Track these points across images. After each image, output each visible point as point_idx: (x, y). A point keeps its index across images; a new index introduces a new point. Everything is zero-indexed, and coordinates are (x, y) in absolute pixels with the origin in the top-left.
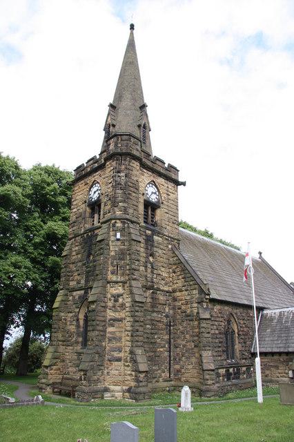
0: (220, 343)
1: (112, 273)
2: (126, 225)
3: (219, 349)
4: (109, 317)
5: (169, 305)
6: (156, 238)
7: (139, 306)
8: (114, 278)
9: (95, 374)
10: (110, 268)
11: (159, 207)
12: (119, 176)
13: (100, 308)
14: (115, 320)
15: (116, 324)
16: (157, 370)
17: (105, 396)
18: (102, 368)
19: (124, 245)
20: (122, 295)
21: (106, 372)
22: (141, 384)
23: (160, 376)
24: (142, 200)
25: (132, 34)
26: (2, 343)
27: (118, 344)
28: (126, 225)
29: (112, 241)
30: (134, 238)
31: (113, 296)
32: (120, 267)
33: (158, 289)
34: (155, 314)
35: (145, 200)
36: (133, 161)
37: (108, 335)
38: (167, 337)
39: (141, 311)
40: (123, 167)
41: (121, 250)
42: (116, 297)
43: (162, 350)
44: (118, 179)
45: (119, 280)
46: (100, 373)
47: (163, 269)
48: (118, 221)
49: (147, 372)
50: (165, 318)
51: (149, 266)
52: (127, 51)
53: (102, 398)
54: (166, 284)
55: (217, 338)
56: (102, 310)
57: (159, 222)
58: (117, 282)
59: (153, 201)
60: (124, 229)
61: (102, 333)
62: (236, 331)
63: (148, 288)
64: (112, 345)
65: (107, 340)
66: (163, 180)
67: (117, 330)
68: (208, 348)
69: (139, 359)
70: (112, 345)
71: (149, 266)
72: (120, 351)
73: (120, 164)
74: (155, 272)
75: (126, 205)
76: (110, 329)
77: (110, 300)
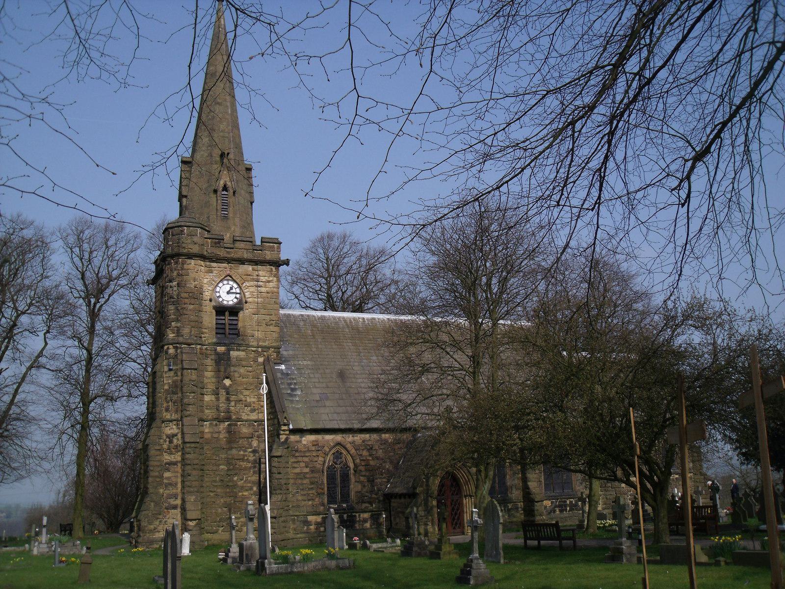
1: (167, 410)
6: (233, 354)
8: (168, 416)
9: (150, 524)
11: (242, 309)
12: (171, 287)
20: (176, 435)
27: (174, 491)
28: (179, 351)
31: (168, 436)
33: (239, 420)
34: (234, 452)
35: (215, 308)
36: (189, 261)
37: (165, 481)
39: (194, 453)
42: (171, 437)
43: (246, 493)
46: (157, 523)
47: (246, 393)
48: (171, 347)
50: (252, 455)
51: (223, 392)
54: (253, 411)
58: (171, 421)
59: (231, 303)
60: (176, 356)
62: (352, 465)
63: (220, 421)
66: (250, 268)
67: (173, 474)
70: (168, 492)
71: (223, 392)
74: (233, 398)
75: (179, 325)
76: (167, 474)
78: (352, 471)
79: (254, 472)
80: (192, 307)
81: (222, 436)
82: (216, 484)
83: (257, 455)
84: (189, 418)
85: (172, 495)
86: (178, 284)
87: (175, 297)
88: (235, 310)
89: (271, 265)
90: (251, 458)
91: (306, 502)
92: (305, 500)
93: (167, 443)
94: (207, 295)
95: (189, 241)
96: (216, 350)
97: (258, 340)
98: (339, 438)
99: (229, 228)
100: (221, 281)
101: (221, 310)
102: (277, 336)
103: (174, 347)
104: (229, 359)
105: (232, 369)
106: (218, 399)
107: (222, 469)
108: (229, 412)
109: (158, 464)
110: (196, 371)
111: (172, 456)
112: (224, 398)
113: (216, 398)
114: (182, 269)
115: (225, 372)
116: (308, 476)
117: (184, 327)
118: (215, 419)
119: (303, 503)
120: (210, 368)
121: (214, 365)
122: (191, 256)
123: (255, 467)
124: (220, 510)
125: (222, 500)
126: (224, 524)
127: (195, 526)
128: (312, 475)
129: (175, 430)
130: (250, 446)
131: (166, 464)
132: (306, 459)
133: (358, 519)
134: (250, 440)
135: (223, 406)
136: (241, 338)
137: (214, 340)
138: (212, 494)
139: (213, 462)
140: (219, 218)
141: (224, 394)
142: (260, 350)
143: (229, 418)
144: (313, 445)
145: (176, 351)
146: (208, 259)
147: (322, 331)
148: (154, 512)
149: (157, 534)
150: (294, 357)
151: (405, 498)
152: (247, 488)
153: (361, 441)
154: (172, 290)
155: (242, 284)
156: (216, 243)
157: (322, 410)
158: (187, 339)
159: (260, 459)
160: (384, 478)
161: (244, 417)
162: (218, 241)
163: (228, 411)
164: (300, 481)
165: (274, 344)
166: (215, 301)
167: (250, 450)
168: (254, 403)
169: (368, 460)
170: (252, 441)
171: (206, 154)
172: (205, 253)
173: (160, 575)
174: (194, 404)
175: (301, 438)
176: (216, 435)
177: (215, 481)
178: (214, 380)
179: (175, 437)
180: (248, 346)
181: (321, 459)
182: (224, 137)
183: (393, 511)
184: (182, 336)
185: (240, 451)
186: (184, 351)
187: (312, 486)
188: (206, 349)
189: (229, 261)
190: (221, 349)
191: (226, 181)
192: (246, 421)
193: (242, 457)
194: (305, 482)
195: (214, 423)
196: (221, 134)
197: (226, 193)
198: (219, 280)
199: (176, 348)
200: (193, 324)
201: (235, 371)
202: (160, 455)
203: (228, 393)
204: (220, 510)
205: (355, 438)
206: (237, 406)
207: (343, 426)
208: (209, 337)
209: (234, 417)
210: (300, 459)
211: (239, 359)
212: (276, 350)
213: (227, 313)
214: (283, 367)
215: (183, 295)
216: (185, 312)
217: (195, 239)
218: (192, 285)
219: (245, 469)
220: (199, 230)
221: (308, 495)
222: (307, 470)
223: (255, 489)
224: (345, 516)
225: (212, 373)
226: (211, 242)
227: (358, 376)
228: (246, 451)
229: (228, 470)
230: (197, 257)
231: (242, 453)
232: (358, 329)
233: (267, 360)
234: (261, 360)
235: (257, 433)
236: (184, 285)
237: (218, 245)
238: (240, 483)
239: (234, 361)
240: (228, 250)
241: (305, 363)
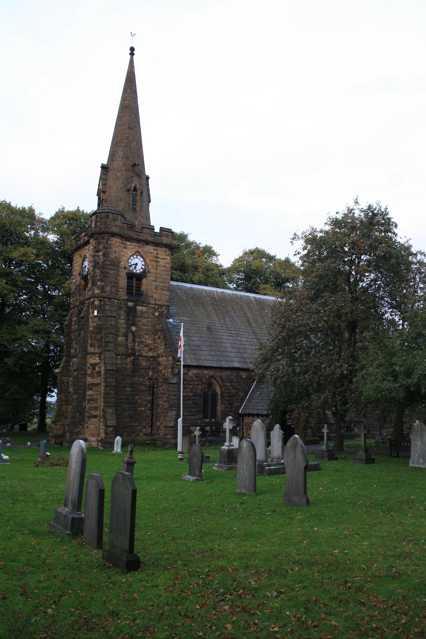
0: (194, 404)
1: (91, 345)
2: (102, 303)
3: (193, 410)
4: (88, 383)
6: (139, 308)
7: (110, 374)
8: (92, 350)
10: (90, 342)
11: (145, 277)
12: (98, 256)
14: (93, 385)
16: (137, 426)
18: (83, 423)
19: (101, 321)
20: (98, 364)
21: (86, 426)
22: (108, 436)
24: (123, 274)
26: (46, 399)
28: (102, 303)
29: (91, 318)
31: (91, 365)
32: (97, 340)
34: (136, 378)
35: (127, 274)
36: (112, 238)
38: (149, 398)
39: (113, 378)
40: (101, 246)
41: (98, 325)
42: (94, 366)
43: (143, 409)
45: (96, 351)
47: (147, 337)
48: (96, 299)
49: (115, 426)
50: (148, 381)
51: (130, 335)
54: (150, 350)
55: (190, 400)
57: (144, 291)
60: (100, 306)
61: (82, 396)
62: (219, 393)
63: (128, 356)
65: (87, 401)
66: (152, 248)
67: (94, 393)
68: (174, 409)
70: (90, 405)
71: (130, 335)
72: (97, 410)
73: (99, 243)
74: (137, 340)
75: (103, 284)
76: (89, 393)
78: (220, 397)
79: (149, 394)
82: (123, 401)
83: (152, 382)
85: (93, 407)
86: (104, 254)
87: (100, 263)
88: (140, 277)
89: (166, 248)
90: (148, 384)
91: (190, 417)
92: (189, 416)
93: (91, 369)
96: (127, 304)
97: (155, 300)
98: (212, 373)
99: (137, 218)
100: (133, 255)
101: (131, 276)
102: (168, 298)
103: (99, 300)
104: (136, 311)
105: (138, 319)
106: (127, 340)
108: (134, 350)
109: (83, 384)
110: (115, 319)
111: (95, 379)
112: (131, 339)
113: (126, 339)
115: (133, 320)
116: (191, 398)
117: (106, 286)
120: (122, 317)
121: (125, 315)
122: (114, 235)
123: (150, 390)
125: (127, 413)
126: (127, 430)
127: (111, 431)
128: (194, 398)
131: (89, 385)
132: (191, 386)
133: (221, 430)
134: (147, 371)
135: (130, 345)
137: (126, 297)
140: (130, 210)
141: (132, 336)
142: (156, 307)
143: (133, 354)
145: (101, 303)
146: (124, 238)
147: (192, 298)
148: (79, 420)
149: (80, 435)
152: (143, 405)
153: (226, 376)
154: (99, 258)
155: (127, 257)
156: (130, 228)
158: (108, 295)
160: (239, 402)
161: (145, 354)
162: (132, 227)
163: (133, 349)
165: (166, 304)
166: (128, 269)
167: (147, 378)
168: (151, 344)
169: (230, 389)
170: (149, 371)
171: (121, 164)
173: (315, 473)
176: (125, 366)
177: (123, 399)
178: (125, 326)
179: (98, 366)
180: (149, 303)
181: (200, 387)
183: (246, 425)
184: (105, 292)
185: (140, 378)
186: (107, 303)
187: (194, 406)
188: (121, 303)
189: (138, 241)
190: (130, 304)
191: (136, 185)
192: (146, 357)
193: (141, 383)
194: (189, 402)
195: (124, 357)
197: (136, 193)
198: (131, 254)
199: (100, 301)
200: (113, 284)
201: (140, 321)
203: (134, 336)
205: (223, 373)
206: (140, 345)
208: (123, 295)
209: (137, 354)
211: (143, 312)
212: (167, 308)
213: (134, 279)
214: (171, 320)
215: (107, 263)
216: (108, 275)
217: (118, 223)
218: (113, 256)
220: (120, 217)
222: (191, 394)
223: (149, 406)
224: (214, 428)
225: (124, 321)
226: (127, 227)
227: (219, 331)
228: (144, 378)
230: (118, 236)
231: (141, 379)
232: (214, 298)
233: (161, 314)
234: (157, 314)
235: (152, 366)
236: (107, 255)
237: (131, 229)
238: (140, 401)
239: (139, 314)
240: (138, 234)
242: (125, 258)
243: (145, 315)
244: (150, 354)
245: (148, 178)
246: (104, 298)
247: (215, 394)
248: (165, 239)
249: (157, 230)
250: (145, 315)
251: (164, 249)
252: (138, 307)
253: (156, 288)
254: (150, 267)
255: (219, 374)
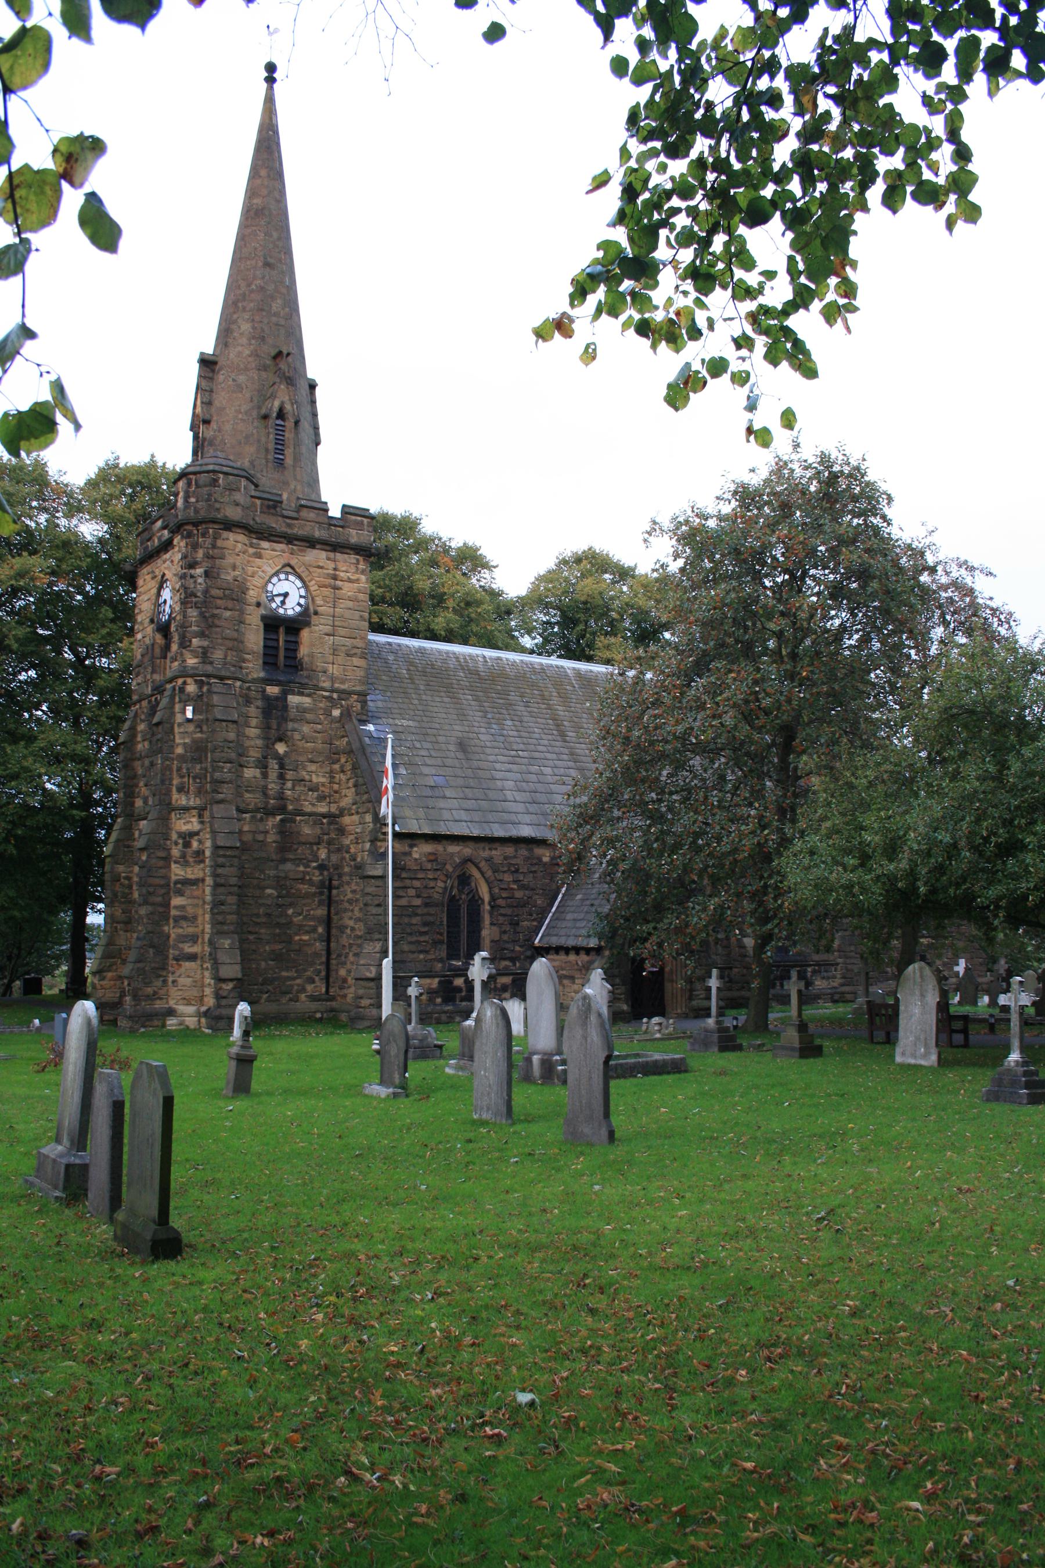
1: (180, 790)
2: (205, 689)
4: (174, 878)
5: (330, 843)
6: (293, 700)
7: (224, 856)
8: (183, 801)
9: (148, 984)
11: (308, 624)
12: (192, 577)
13: (154, 861)
14: (186, 882)
15: (189, 890)
16: (294, 979)
17: (168, 1022)
19: (201, 732)
20: (197, 833)
21: (170, 979)
23: (303, 990)
24: (254, 619)
25: (270, 101)
28: (205, 689)
29: (180, 725)
30: (219, 717)
33: (299, 812)
34: (289, 866)
35: (264, 618)
36: (225, 534)
38: (321, 912)
39: (232, 866)
40: (200, 554)
41: (194, 741)
42: (187, 837)
43: (306, 938)
44: (190, 583)
45: (191, 803)
46: (159, 983)
47: (312, 767)
48: (189, 680)
50: (317, 873)
51: (273, 764)
52: (73, 414)
53: (164, 1025)
54: (322, 798)
55: (417, 915)
56: (161, 863)
57: (306, 659)
60: (200, 697)
61: (161, 910)
62: (487, 898)
63: (270, 813)
64: (180, 931)
65: (171, 921)
66: (323, 555)
67: (190, 901)
69: (222, 957)
70: (180, 931)
71: (273, 764)
72: (195, 942)
73: (195, 546)
74: (290, 775)
76: (176, 901)
77: (176, 844)
78: (487, 907)
79: (321, 903)
80: (228, 614)
81: (270, 838)
84: (222, 806)
85: (186, 936)
86: (206, 572)
89: (357, 554)
93: (180, 846)
94: (252, 594)
95: (226, 499)
96: (264, 691)
97: (333, 679)
98: (467, 850)
99: (286, 483)
100: (276, 574)
101: (273, 624)
102: (362, 673)
104: (285, 707)
105: (290, 725)
106: (265, 775)
107: (270, 895)
109: (162, 882)
111: (189, 870)
114: (214, 546)
115: (278, 730)
118: (257, 810)
119: (411, 956)
120: (254, 722)
122: (229, 525)
123: (321, 893)
124: (263, 964)
128: (425, 910)
129: (194, 825)
130: (316, 858)
131: (176, 882)
135: (273, 787)
136: (305, 673)
137: (262, 675)
138: (251, 937)
139: (255, 882)
142: (335, 696)
143: (282, 809)
144: (430, 861)
145: (201, 688)
150: (388, 712)
151: (577, 954)
156: (269, 507)
157: (442, 804)
159: (330, 880)
161: (308, 808)
162: (273, 505)
163: (281, 796)
164: (406, 920)
165: (358, 688)
166: (266, 607)
168: (323, 785)
171: (247, 352)
172: (251, 522)
174: (230, 782)
175: (411, 846)
176: (260, 837)
177: (258, 915)
178: (259, 742)
180: (317, 688)
182: (277, 325)
184: (211, 663)
186: (215, 690)
187: (426, 929)
188: (249, 689)
189: (289, 539)
190: (273, 690)
191: (283, 403)
192: (310, 814)
193: (300, 876)
195: (259, 816)
196: (274, 319)
199: (200, 684)
200: (230, 644)
201: (295, 730)
202: (164, 867)
203: (282, 766)
204: (263, 964)
205: (494, 852)
207: (476, 833)
208: (254, 669)
209: (290, 807)
210: (408, 882)
211: (302, 710)
213: (282, 630)
214: (371, 727)
215: (215, 592)
216: (217, 622)
218: (228, 576)
219: (307, 895)
220: (243, 482)
221: (418, 942)
222: (418, 902)
223: (320, 930)
225: (257, 731)
229: (278, 897)
231: (302, 868)
232: (477, 673)
233: (347, 713)
234: (336, 713)
238: (297, 920)
239: (293, 713)
241: (405, 723)
242: (257, 581)
243: (308, 716)
244: (322, 808)
245: (312, 386)
246: (208, 676)
247: (475, 902)
248: (353, 532)
249: (335, 512)
250: (308, 716)
251: (353, 558)
252: (290, 697)
253: (335, 652)
254: (319, 601)
255: (486, 854)
